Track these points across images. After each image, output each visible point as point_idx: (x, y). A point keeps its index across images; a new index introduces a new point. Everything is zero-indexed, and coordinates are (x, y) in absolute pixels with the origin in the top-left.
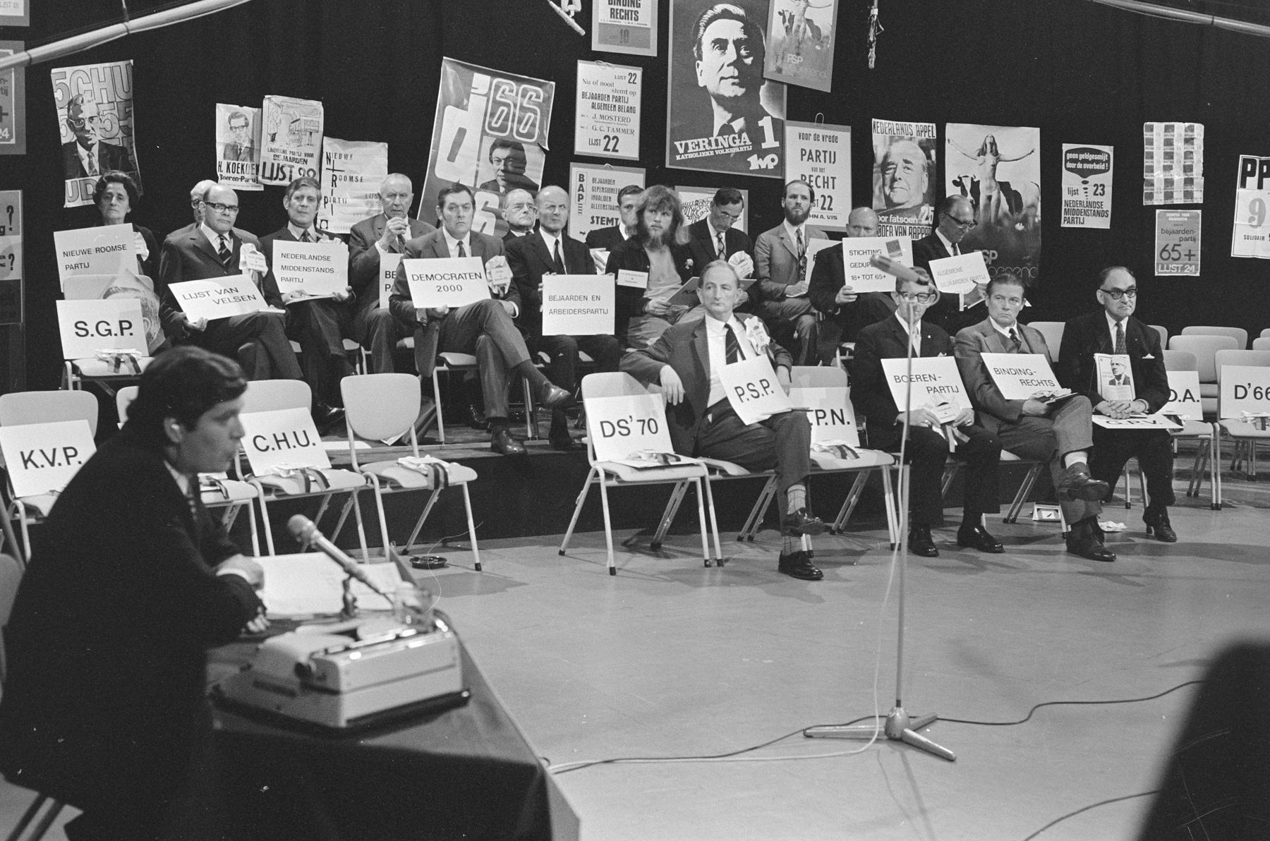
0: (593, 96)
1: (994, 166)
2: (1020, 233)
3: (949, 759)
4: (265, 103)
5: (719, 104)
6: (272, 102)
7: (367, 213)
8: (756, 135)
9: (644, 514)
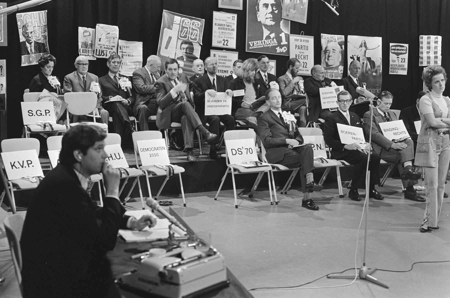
0: (219, 25)
1: (365, 51)
2: (374, 77)
3: (387, 288)
4: (97, 27)
5: (265, 28)
6: (99, 26)
7: (135, 68)
8: (279, 40)
9: (249, 184)
